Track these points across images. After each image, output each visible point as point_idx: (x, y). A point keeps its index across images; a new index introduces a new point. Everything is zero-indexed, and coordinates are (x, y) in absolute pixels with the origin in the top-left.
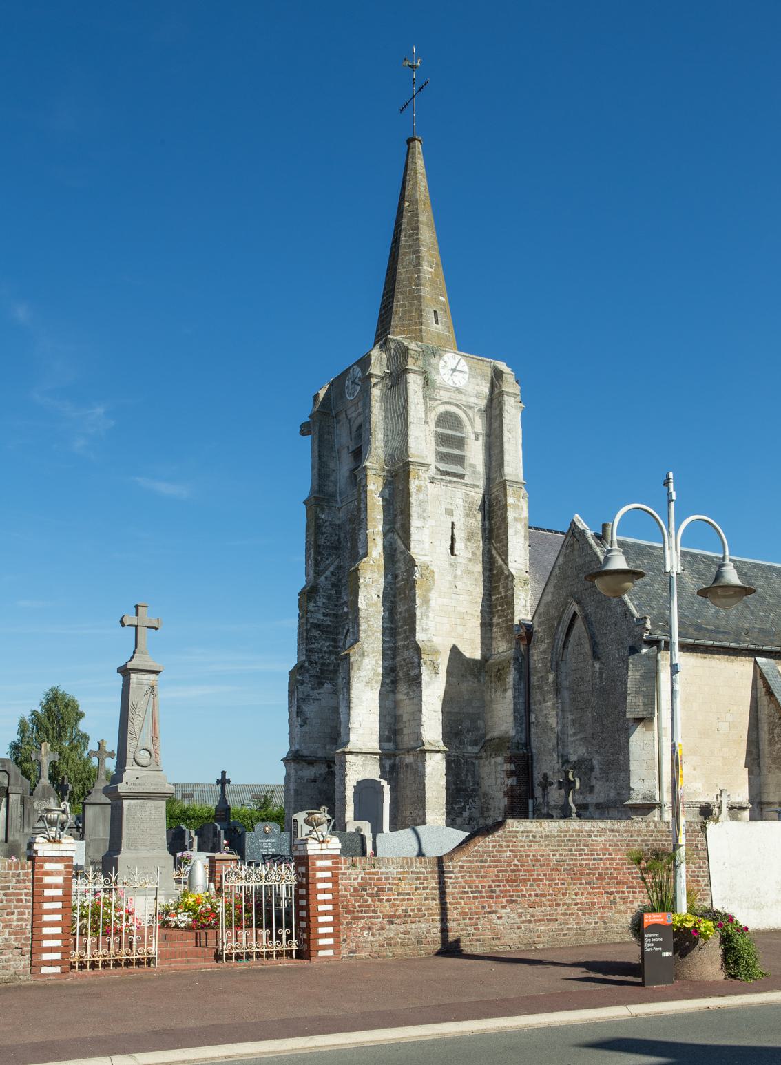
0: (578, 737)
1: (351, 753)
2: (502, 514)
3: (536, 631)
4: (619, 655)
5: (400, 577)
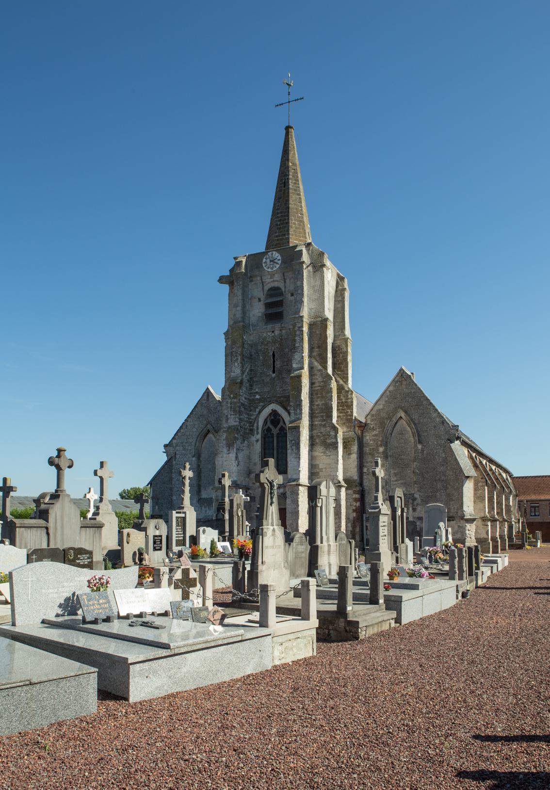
0: (399, 482)
1: (301, 485)
2: (343, 356)
3: (369, 424)
4: (437, 442)
5: (317, 384)
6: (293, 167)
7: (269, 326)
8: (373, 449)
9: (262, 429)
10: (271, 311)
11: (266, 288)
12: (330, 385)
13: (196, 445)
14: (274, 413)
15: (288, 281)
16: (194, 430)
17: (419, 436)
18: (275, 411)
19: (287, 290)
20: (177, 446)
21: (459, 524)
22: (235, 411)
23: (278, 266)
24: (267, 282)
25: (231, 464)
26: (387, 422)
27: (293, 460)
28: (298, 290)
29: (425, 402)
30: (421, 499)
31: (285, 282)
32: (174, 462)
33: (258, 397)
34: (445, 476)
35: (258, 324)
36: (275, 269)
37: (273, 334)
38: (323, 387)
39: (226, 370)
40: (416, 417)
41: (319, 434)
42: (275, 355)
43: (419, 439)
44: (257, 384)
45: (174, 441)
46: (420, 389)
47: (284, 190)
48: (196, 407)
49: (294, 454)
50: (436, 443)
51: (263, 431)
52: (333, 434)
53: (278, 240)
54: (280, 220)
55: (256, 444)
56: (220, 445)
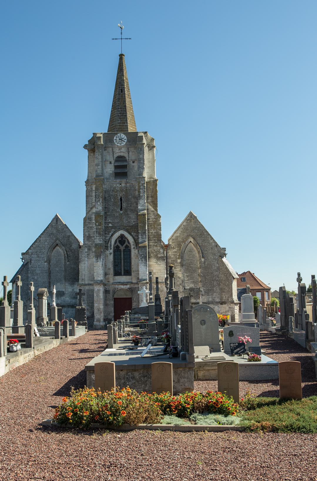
3: (171, 245)
5: (151, 220)
6: (127, 81)
7: (118, 181)
8: (174, 260)
9: (114, 245)
10: (119, 171)
11: (116, 156)
12: (159, 221)
13: (47, 253)
14: (122, 236)
15: (130, 153)
16: (46, 243)
17: (202, 253)
18: (123, 235)
19: (130, 159)
20: (32, 254)
21: (229, 306)
22: (99, 234)
23: (124, 143)
24: (116, 152)
25: (98, 269)
26: (182, 244)
27: (143, 267)
28: (140, 160)
29: (205, 233)
30: (204, 292)
31: (128, 154)
32: (30, 266)
33: (110, 225)
34: (219, 278)
35: (109, 178)
36: (122, 145)
37: (120, 186)
38: (155, 221)
39: (86, 206)
40: (200, 242)
41: (153, 251)
42: (122, 199)
43: (202, 255)
44: (109, 217)
45: (30, 251)
46: (202, 225)
47: (122, 94)
48: (48, 227)
49: (143, 264)
50: (212, 258)
51: (114, 248)
52: (162, 251)
53: (120, 125)
54: (120, 113)
55: (110, 256)
56: (82, 256)
